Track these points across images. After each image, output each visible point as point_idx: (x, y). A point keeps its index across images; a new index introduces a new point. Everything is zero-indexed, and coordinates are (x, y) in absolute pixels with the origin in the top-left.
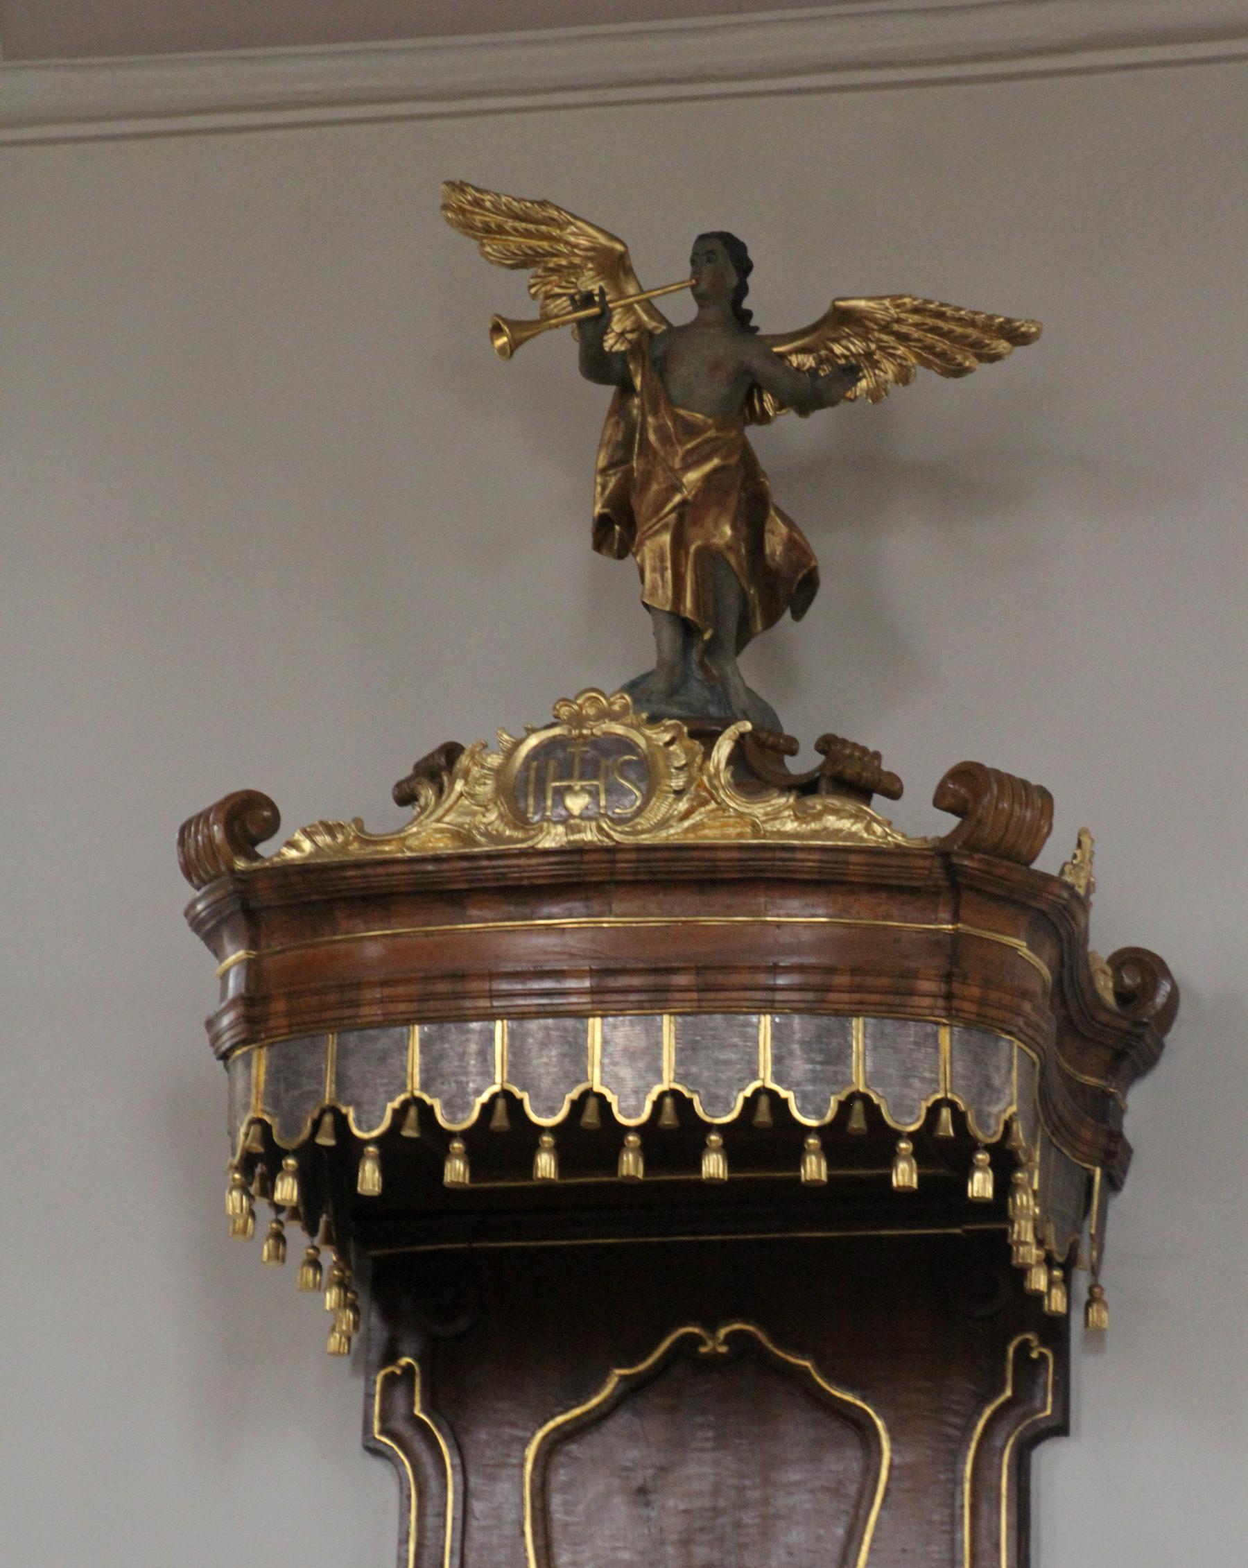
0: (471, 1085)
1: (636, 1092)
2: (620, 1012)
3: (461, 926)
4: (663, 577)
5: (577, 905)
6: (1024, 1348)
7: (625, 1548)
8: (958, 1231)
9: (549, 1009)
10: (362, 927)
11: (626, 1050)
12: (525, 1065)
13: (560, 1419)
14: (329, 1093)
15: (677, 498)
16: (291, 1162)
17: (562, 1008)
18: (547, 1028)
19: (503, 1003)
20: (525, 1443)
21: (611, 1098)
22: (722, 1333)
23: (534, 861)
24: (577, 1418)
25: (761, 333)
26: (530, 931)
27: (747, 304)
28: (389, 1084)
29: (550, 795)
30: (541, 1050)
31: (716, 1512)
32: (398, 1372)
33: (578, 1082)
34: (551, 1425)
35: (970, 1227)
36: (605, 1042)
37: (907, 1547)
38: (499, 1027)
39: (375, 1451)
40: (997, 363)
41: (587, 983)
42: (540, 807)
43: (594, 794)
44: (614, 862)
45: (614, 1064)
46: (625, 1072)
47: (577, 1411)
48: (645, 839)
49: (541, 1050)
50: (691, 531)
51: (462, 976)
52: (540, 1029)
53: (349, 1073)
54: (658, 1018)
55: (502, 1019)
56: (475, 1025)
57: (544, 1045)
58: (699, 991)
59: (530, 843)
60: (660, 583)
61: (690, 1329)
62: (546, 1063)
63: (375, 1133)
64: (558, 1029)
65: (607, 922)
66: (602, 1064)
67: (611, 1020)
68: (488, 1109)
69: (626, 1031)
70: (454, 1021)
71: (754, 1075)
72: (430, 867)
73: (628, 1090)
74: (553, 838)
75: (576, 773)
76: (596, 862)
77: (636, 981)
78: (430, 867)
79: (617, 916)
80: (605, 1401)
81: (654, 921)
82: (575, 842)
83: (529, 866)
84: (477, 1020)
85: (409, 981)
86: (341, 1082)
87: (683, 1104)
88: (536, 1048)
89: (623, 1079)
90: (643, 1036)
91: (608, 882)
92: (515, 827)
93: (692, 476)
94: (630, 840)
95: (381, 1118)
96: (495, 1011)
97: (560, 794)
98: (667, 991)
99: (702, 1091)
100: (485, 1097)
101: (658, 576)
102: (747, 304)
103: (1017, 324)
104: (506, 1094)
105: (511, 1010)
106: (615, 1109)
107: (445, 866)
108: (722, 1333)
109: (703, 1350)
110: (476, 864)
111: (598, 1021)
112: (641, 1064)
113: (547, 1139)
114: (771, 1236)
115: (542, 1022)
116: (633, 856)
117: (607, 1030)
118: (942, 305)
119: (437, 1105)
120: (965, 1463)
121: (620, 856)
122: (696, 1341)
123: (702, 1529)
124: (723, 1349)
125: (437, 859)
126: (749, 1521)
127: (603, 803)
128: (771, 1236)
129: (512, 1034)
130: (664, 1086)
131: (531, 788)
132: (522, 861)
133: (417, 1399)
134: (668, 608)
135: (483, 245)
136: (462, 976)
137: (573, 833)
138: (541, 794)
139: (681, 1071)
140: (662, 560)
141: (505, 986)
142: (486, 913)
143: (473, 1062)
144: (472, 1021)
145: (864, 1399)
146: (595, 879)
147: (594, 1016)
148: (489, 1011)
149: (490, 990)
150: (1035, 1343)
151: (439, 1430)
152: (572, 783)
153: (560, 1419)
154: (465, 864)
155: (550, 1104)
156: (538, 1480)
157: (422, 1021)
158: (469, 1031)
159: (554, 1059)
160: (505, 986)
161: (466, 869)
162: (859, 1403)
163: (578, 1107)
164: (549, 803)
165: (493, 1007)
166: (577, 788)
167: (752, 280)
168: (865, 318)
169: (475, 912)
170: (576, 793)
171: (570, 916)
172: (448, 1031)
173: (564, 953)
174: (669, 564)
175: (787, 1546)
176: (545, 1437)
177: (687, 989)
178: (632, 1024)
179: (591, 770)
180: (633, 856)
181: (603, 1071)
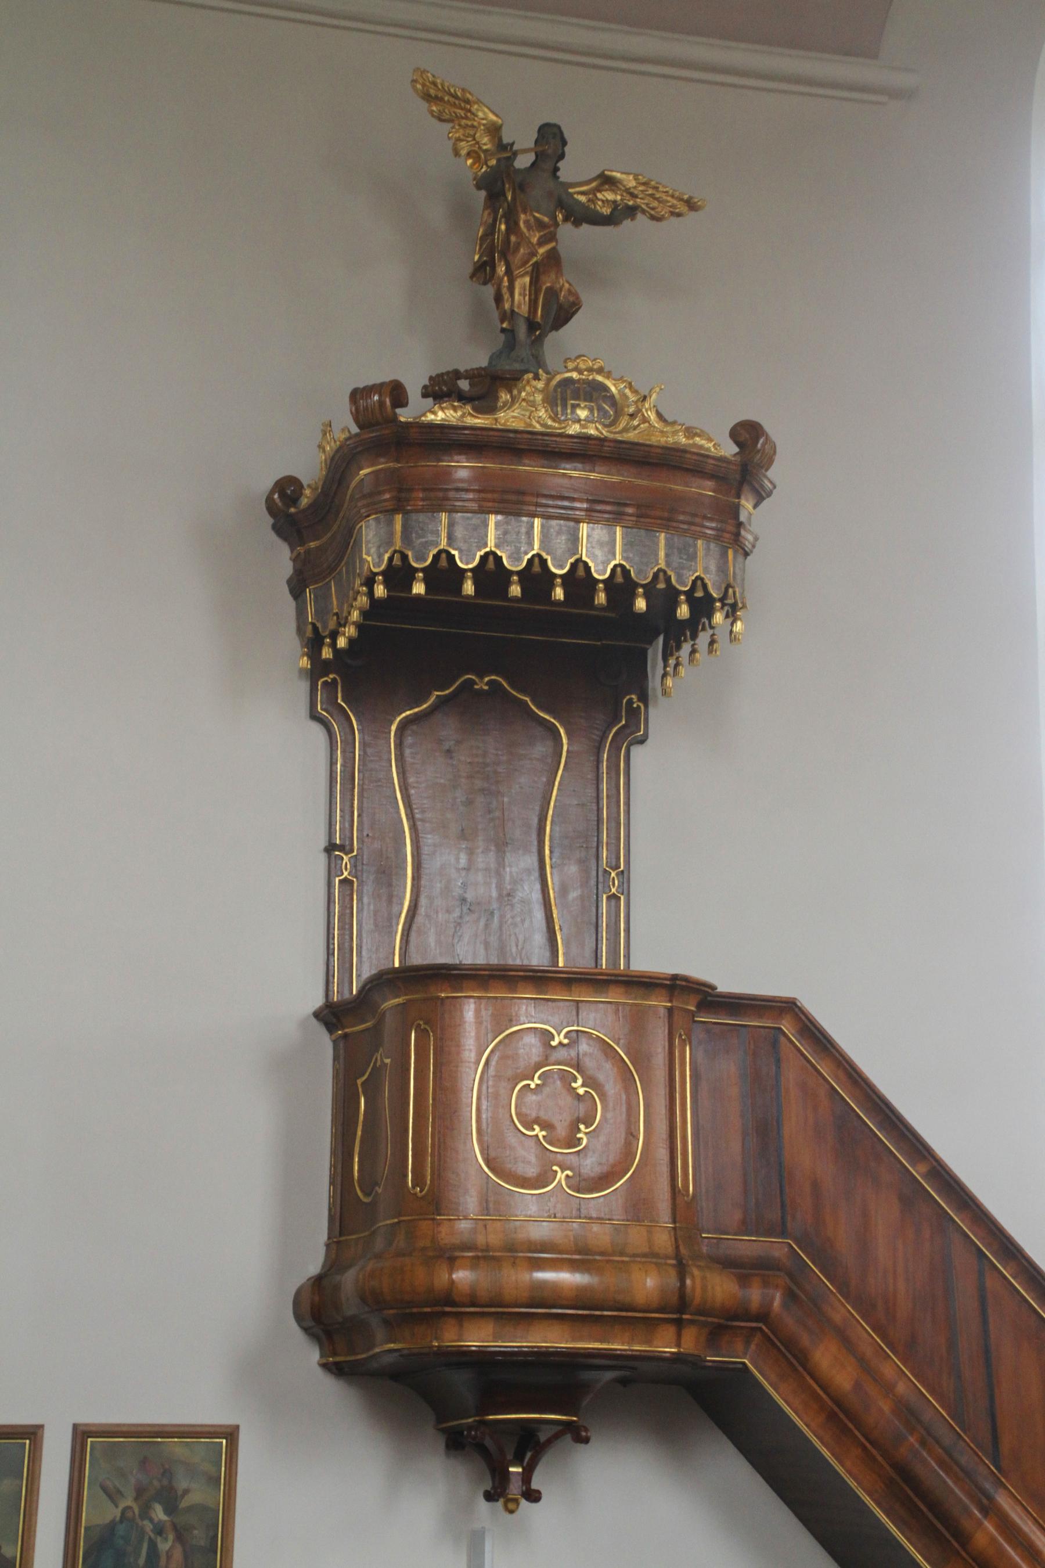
0: (522, 548)
1: (603, 563)
2: (597, 522)
3: (521, 468)
4: (524, 299)
5: (579, 466)
6: (630, 702)
7: (441, 777)
8: (599, 643)
9: (566, 516)
10: (464, 460)
11: (598, 541)
12: (549, 542)
13: (408, 713)
14: (443, 544)
15: (535, 259)
16: (421, 575)
17: (570, 516)
18: (560, 525)
19: (542, 510)
20: (391, 723)
21: (591, 564)
22: (486, 679)
23: (564, 440)
24: (416, 714)
25: (561, 180)
26: (554, 475)
27: (560, 164)
28: (479, 542)
29: (569, 407)
30: (557, 536)
31: (486, 765)
32: (329, 680)
33: (575, 554)
34: (404, 715)
35: (604, 642)
36: (588, 536)
37: (576, 789)
38: (537, 522)
39: (314, 716)
40: (680, 218)
41: (585, 506)
42: (564, 413)
43: (591, 410)
44: (602, 446)
45: (593, 547)
46: (598, 553)
47: (416, 710)
48: (619, 437)
49: (557, 536)
50: (543, 278)
51: (523, 493)
52: (557, 525)
53: (456, 534)
54: (614, 527)
55: (538, 518)
56: (525, 519)
57: (559, 533)
58: (637, 517)
59: (563, 430)
60: (523, 302)
61: (470, 676)
62: (561, 542)
63: (470, 566)
64: (566, 526)
65: (593, 476)
66: (587, 547)
67: (591, 525)
68: (530, 561)
69: (600, 532)
70: (514, 516)
71: (658, 564)
72: (511, 435)
73: (599, 561)
74: (574, 429)
75: (582, 397)
76: (595, 445)
77: (608, 508)
78: (511, 435)
79: (597, 473)
80: (429, 707)
81: (615, 479)
82: (584, 433)
83: (562, 442)
84: (525, 516)
85: (493, 491)
86: (450, 538)
87: (626, 572)
88: (554, 534)
89: (597, 556)
90: (607, 535)
91: (595, 456)
92: (554, 421)
93: (542, 251)
94: (611, 436)
95: (474, 559)
96: (537, 513)
97: (574, 407)
98: (624, 515)
99: (635, 567)
100: (529, 556)
101: (522, 298)
102: (560, 164)
103: (696, 200)
104: (538, 555)
105: (545, 514)
106: (593, 570)
107: (519, 436)
108: (486, 679)
109: (476, 687)
110: (535, 437)
111: (585, 525)
112: (606, 549)
113: (559, 580)
114: (482, 633)
115: (558, 522)
116: (612, 444)
117: (589, 530)
118: (657, 183)
119: (410, 554)
120: (604, 753)
121: (606, 444)
122: (472, 682)
123: (478, 772)
124: (486, 688)
125: (516, 431)
126: (501, 771)
127: (596, 415)
128: (482, 633)
129: (543, 526)
130: (617, 562)
131: (559, 402)
132: (558, 439)
133: (339, 695)
134: (526, 315)
135: (430, 106)
136: (523, 493)
137: (583, 429)
138: (564, 406)
139: (625, 555)
140: (525, 290)
141: (544, 501)
142: (532, 463)
143: (523, 537)
144: (523, 516)
145: (554, 718)
146: (590, 453)
147: (583, 522)
148: (534, 513)
149: (537, 503)
150: (635, 700)
151: (351, 711)
152: (581, 403)
153: (408, 713)
154: (530, 436)
155: (561, 563)
156: (398, 741)
157: (497, 513)
158: (521, 521)
159: (564, 541)
160: (544, 501)
161: (530, 439)
162: (552, 720)
163: (574, 566)
164: (569, 411)
165: (536, 511)
166: (582, 405)
167: (566, 149)
168: (619, 183)
169: (527, 461)
170: (583, 408)
171: (575, 470)
172: (511, 520)
173: (570, 488)
174: (527, 293)
175: (520, 783)
176: (400, 721)
177: (631, 515)
178: (602, 529)
179: (588, 398)
180: (612, 444)
181: (587, 551)
